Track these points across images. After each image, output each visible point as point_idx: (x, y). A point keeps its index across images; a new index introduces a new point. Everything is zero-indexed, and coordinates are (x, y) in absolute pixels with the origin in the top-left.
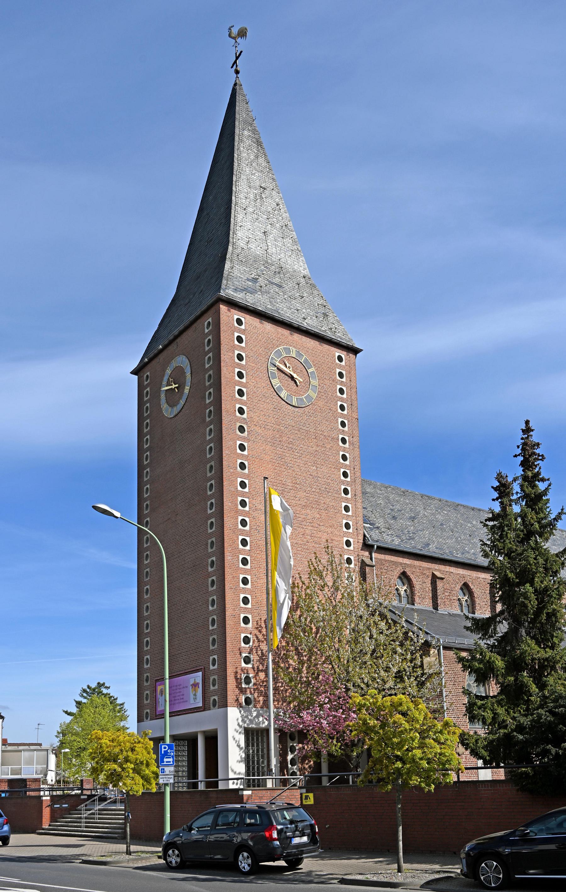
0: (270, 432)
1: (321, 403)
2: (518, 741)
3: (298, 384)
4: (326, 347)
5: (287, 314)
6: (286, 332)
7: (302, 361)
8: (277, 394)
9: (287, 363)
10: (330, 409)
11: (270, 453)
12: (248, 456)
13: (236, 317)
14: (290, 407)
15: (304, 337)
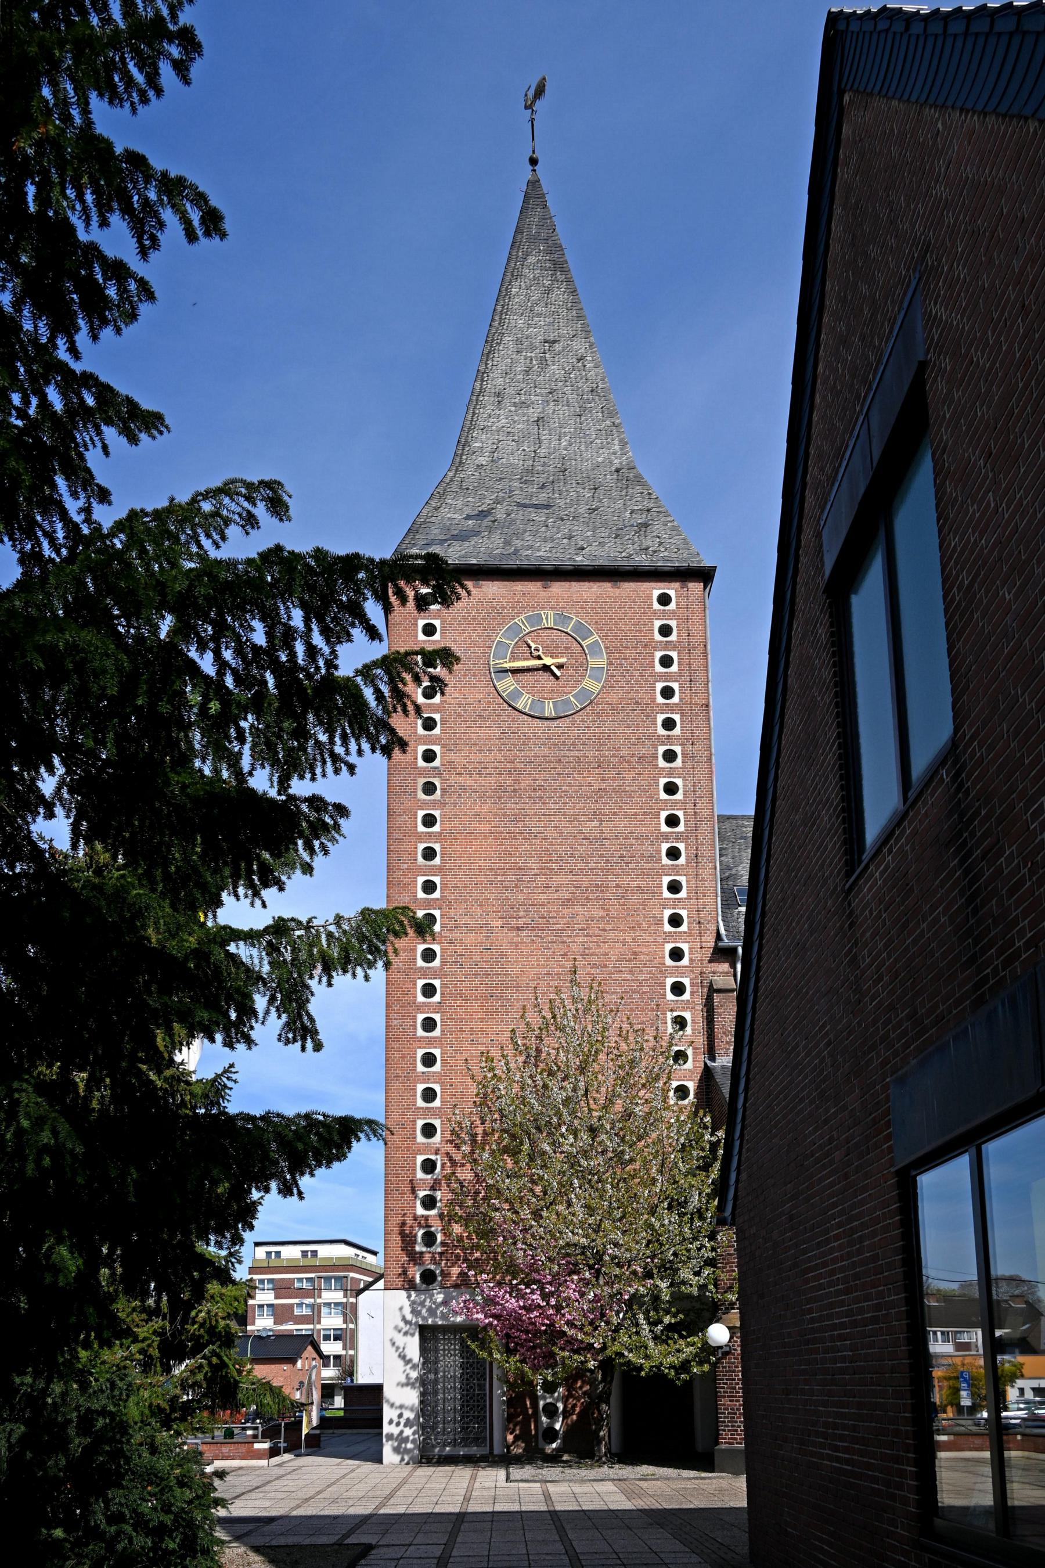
1: (613, 698)
4: (629, 588)
6: (532, 588)
7: (568, 630)
8: (510, 706)
9: (530, 642)
10: (637, 703)
12: (440, 834)
13: (656, 593)
15: (574, 584)
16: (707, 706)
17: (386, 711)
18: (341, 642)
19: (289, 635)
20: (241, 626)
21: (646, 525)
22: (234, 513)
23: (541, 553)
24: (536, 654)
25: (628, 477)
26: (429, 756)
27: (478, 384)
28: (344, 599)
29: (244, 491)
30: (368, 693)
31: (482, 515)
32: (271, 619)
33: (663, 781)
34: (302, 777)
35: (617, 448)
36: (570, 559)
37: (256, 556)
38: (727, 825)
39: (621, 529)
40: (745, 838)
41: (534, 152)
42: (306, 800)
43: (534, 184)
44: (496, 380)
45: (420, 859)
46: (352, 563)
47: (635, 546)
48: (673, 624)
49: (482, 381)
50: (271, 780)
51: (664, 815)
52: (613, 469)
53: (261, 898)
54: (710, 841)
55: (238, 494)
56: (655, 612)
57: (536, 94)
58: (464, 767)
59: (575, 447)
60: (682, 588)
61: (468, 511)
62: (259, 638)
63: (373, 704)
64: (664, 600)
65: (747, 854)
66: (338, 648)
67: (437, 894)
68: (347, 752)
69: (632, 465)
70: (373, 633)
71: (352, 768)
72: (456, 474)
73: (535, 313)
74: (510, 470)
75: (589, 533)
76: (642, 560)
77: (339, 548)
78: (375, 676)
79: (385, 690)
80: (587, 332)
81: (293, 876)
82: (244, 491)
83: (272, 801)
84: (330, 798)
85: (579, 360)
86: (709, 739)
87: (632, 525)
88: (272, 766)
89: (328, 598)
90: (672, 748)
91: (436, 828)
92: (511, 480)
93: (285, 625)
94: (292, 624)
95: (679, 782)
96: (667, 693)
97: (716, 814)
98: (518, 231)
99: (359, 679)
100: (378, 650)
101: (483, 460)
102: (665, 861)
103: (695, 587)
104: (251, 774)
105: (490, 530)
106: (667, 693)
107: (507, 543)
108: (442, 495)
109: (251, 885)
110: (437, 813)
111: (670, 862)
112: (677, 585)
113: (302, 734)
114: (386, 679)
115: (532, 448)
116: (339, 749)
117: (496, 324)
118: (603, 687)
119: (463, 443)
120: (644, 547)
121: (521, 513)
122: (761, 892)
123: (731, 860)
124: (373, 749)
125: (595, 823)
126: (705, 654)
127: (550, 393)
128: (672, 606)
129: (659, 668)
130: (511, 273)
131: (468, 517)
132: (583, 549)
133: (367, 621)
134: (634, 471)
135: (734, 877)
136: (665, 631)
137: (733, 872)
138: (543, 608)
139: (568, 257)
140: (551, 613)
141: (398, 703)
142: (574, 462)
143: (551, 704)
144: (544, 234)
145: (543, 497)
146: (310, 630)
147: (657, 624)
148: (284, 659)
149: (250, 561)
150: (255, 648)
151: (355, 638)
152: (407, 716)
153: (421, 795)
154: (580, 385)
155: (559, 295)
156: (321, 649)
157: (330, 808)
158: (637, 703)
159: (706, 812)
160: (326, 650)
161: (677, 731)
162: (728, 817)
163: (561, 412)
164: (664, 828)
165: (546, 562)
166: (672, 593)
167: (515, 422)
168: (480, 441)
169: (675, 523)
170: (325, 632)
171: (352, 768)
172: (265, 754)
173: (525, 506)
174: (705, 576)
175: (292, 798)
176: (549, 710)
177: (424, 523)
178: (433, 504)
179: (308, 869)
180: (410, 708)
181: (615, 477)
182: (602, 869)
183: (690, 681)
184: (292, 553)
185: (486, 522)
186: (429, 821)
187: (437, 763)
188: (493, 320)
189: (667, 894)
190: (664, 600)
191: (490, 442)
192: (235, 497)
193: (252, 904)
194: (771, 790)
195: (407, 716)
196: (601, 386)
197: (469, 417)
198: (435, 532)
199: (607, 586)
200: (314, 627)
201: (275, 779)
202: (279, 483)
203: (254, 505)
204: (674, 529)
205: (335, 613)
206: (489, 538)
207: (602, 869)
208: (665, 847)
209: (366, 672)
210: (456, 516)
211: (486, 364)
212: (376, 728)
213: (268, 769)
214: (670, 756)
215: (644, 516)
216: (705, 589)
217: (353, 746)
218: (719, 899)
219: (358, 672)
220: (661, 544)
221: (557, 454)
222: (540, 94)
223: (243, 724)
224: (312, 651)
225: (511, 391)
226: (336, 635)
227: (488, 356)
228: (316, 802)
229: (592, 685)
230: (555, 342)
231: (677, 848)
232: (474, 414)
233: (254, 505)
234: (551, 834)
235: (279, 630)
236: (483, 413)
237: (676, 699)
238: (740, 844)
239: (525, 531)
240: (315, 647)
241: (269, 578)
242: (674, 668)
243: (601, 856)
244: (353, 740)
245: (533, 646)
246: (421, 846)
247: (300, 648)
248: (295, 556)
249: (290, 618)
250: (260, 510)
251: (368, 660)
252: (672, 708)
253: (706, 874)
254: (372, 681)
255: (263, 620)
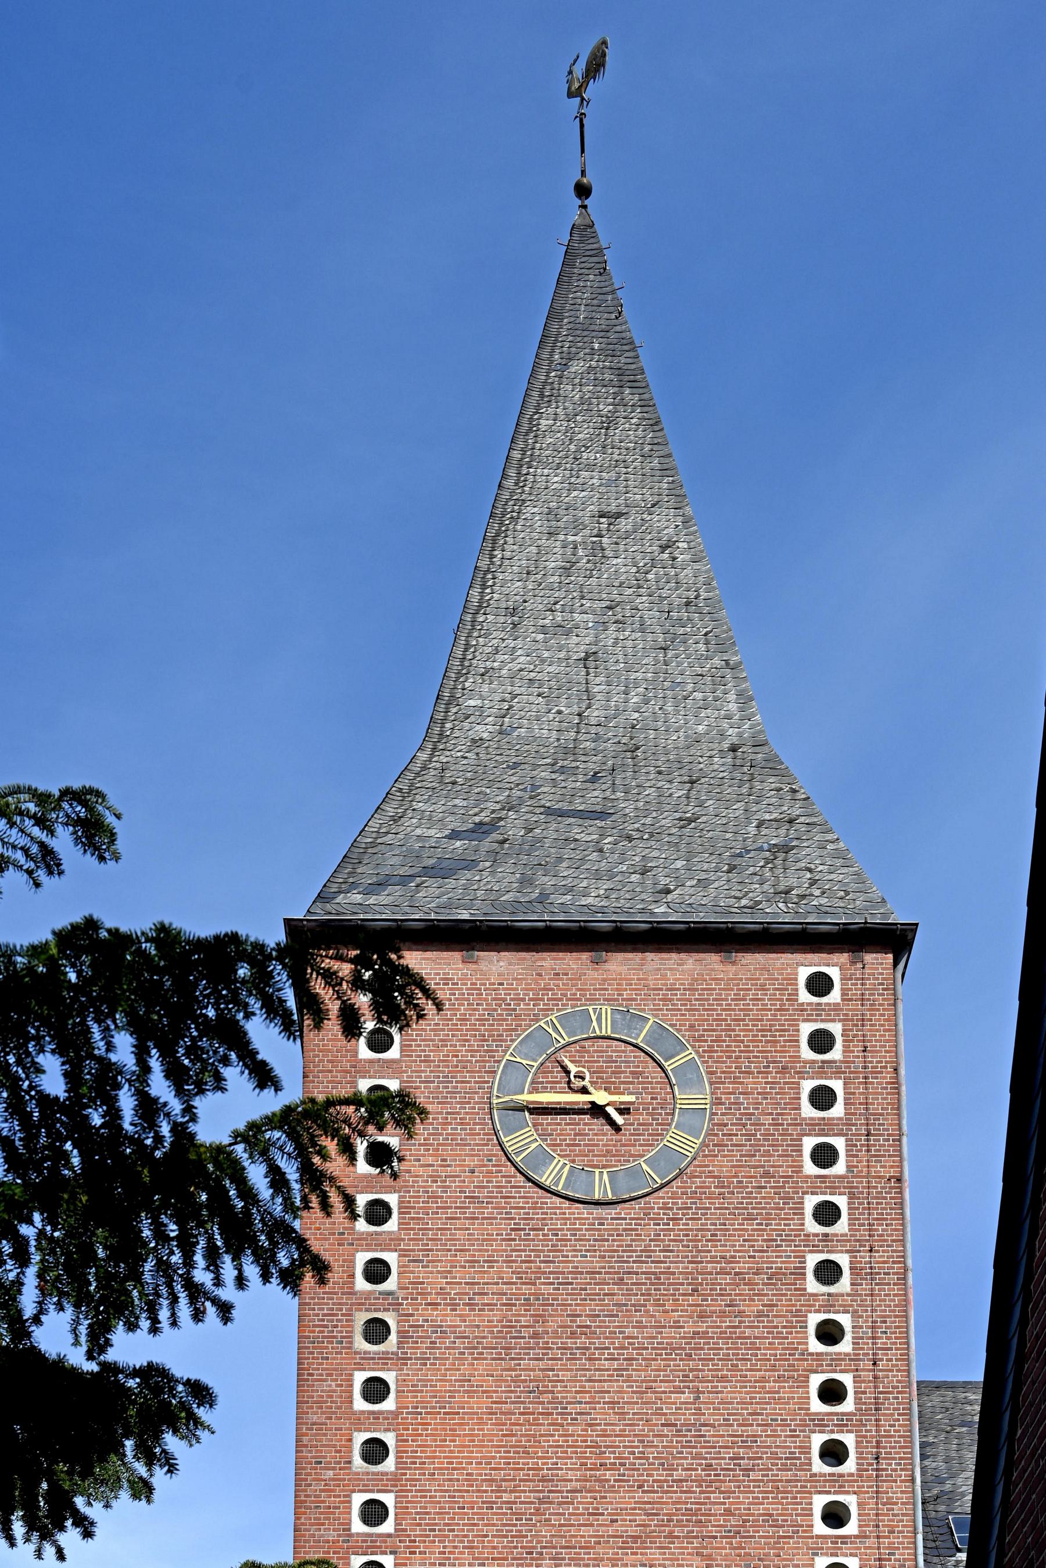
0: (495, 1315)
1: (722, 1165)
2: (147, 1061)
3: (619, 1119)
4: (752, 962)
5: (592, 901)
6: (573, 963)
7: (639, 1041)
8: (529, 1179)
9: (567, 1062)
10: (766, 1174)
11: (490, 1384)
12: (395, 1414)
13: (804, 973)
14: (584, 1211)
15: (650, 956)
16: (899, 1180)
17: (289, 1206)
18: (201, 1092)
19: (108, 1075)
20: (19, 1062)
21: (786, 849)
22: (14, 847)
23: (590, 900)
24: (578, 1084)
25: (753, 761)
26: (377, 1272)
27: (475, 593)
28: (211, 1013)
29: (32, 807)
30: (257, 1175)
31: (481, 830)
32: (74, 1048)
33: (814, 1319)
34: (132, 1327)
35: (733, 707)
36: (643, 911)
37: (50, 937)
38: (936, 1399)
39: (740, 855)
40: (969, 1424)
41: (583, 173)
42: (136, 1373)
43: (584, 231)
44: (509, 586)
45: (358, 1461)
46: (226, 949)
47: (766, 887)
48: (836, 1029)
49: (484, 586)
50: (74, 1331)
51: (816, 1380)
52: (726, 745)
53: (55, 1544)
54: (902, 1429)
55: (21, 813)
56: (802, 1008)
57: (588, 70)
58: (442, 1292)
59: (654, 706)
60: (853, 963)
61: (454, 823)
62: (52, 1078)
63: (265, 1192)
64: (819, 985)
65: (970, 1457)
66: (197, 1102)
67: (388, 1527)
68: (218, 1282)
69: (762, 737)
70: (264, 1077)
71: (225, 1310)
72: (432, 755)
73: (583, 464)
74: (533, 747)
75: (679, 864)
76: (779, 913)
77: (200, 925)
78: (270, 1143)
79: (291, 1171)
80: (679, 499)
81: (114, 1503)
82: (32, 807)
83: (74, 1373)
84: (180, 1371)
85: (663, 548)
86: (903, 1242)
87: (760, 849)
88: (77, 1306)
89: (185, 1010)
90: (832, 1257)
91: (389, 1404)
92: (535, 767)
93: (100, 1060)
94: (113, 1057)
95: (845, 1320)
96: (824, 1156)
97: (914, 1379)
98: (553, 315)
99: (240, 1148)
100: (270, 1103)
101: (483, 731)
102: (818, 1466)
103: (878, 962)
104: (37, 1320)
105: (495, 858)
106: (824, 1156)
107: (526, 881)
108: (407, 795)
109: (32, 1524)
110: (390, 1377)
111: (828, 1469)
112: (844, 958)
113: (129, 1251)
114: (289, 1148)
115: (575, 709)
116: (202, 1276)
117: (509, 483)
118: (704, 1144)
119: (445, 700)
120: (782, 888)
121: (554, 826)
122: (996, 1532)
123: (942, 1465)
124: (266, 1277)
125: (687, 1396)
126: (896, 1084)
127: (610, 608)
128: (835, 996)
129: (808, 1110)
130: (538, 392)
131: (454, 835)
132: (668, 892)
133: (254, 1053)
134: (765, 749)
135: (951, 1497)
136: (821, 1041)
137: (948, 1487)
138: (593, 1000)
139: (644, 361)
140: (606, 1010)
141: (312, 1191)
142: (652, 734)
143: (605, 1177)
144: (601, 321)
145: (594, 797)
146: (146, 1070)
147: (806, 1029)
148: (97, 1120)
149: (36, 951)
150: (45, 1101)
151: (229, 1084)
152: (329, 1215)
153: (361, 1344)
154: (665, 593)
155: (629, 430)
156: (165, 1104)
157: (180, 1388)
158: (766, 1174)
159: (895, 1377)
160: (176, 1106)
161: (842, 1226)
162: (939, 1386)
163: (630, 643)
164: (817, 1406)
165: (599, 917)
166: (834, 973)
167: (543, 661)
168: (479, 696)
169: (841, 845)
170: (175, 1074)
171: (225, 1310)
172: (67, 1282)
173: (562, 814)
174: (896, 940)
175: (110, 1369)
176: (601, 1187)
177: (373, 844)
178: (390, 810)
179: (143, 1490)
180: (335, 1198)
181: (729, 760)
182: (699, 1482)
183: (866, 1131)
184: (114, 933)
185: (488, 843)
186: (376, 1390)
187: (390, 1284)
188: (504, 476)
189: (820, 1528)
190: (819, 985)
191: (497, 697)
192: (18, 819)
193: (39, 1554)
194: (1015, 1341)
195: (329, 1215)
196: (704, 595)
197: (459, 652)
198: (392, 863)
199: (712, 960)
200: (155, 1063)
201: (83, 1330)
202: (98, 794)
203: (52, 832)
204: (838, 854)
205: (193, 1039)
206: (493, 873)
207: (699, 1482)
208: (818, 1440)
209: (252, 1135)
210: (432, 832)
211: (492, 557)
212: (270, 1238)
213: (69, 1312)
214: (828, 1272)
215: (782, 832)
216: (896, 964)
217: (228, 1271)
218: (920, 1537)
219: (238, 1136)
220: (813, 882)
221: (621, 719)
222: (597, 71)
223: (25, 1230)
224: (149, 1108)
225: (536, 604)
226: (190, 1081)
227: (494, 541)
228: (154, 1375)
229: (683, 1141)
230: (619, 515)
231: (841, 1443)
232: (467, 646)
233: (52, 832)
234: (602, 1414)
235: (90, 1068)
236: (484, 645)
237: (840, 1168)
238: (959, 1437)
239: (560, 859)
240: (156, 1100)
241: (73, 977)
242: (838, 1110)
243: (698, 1456)
244: (227, 1259)
245: (573, 1069)
246: (360, 1438)
247: (127, 1101)
248: (121, 940)
249: (110, 1047)
250: (63, 841)
251: (256, 1115)
252: (833, 1185)
253: (896, 1491)
254: (264, 1153)
255: (60, 1051)
